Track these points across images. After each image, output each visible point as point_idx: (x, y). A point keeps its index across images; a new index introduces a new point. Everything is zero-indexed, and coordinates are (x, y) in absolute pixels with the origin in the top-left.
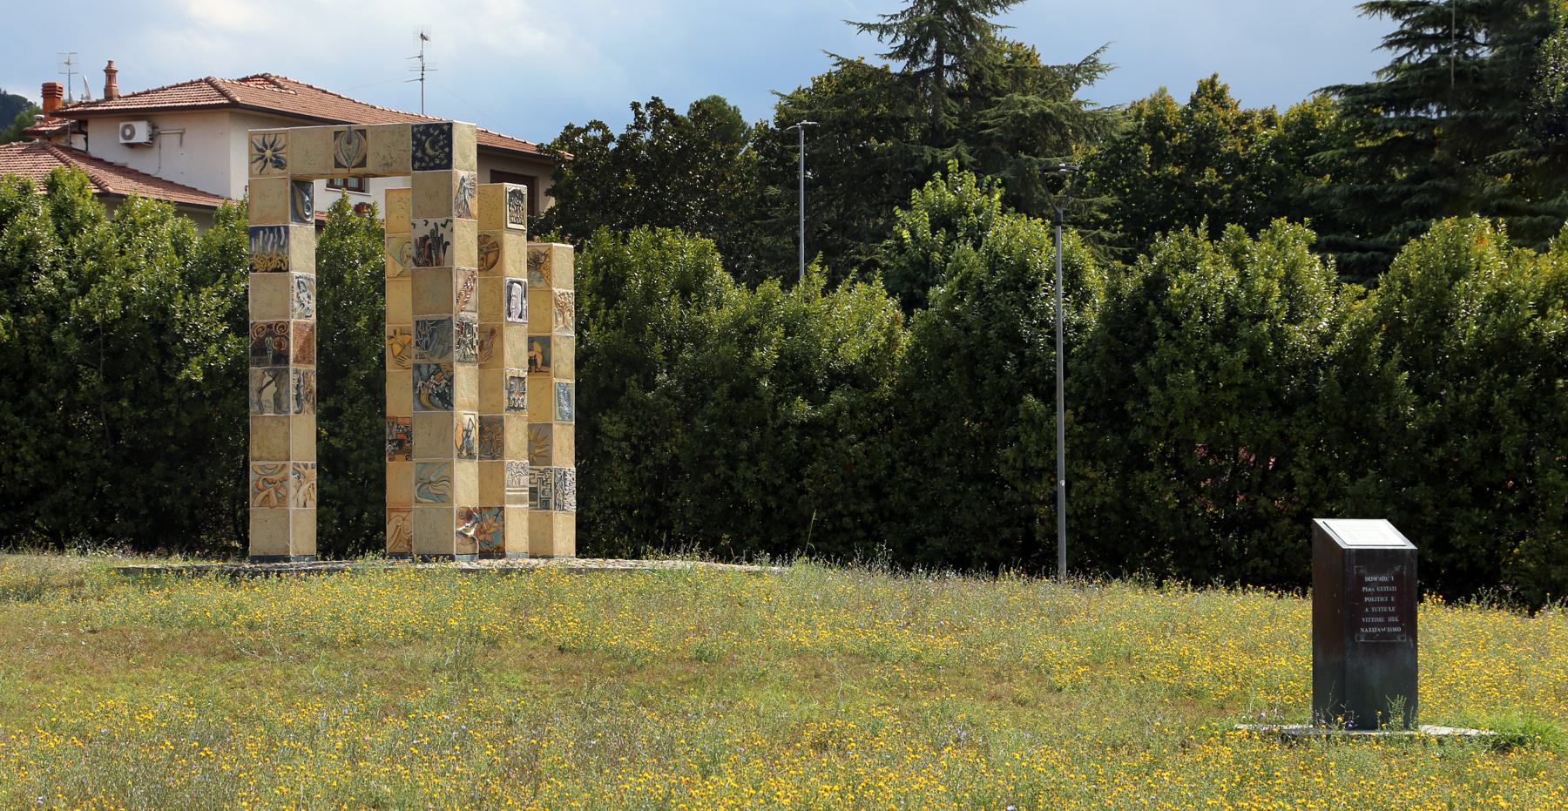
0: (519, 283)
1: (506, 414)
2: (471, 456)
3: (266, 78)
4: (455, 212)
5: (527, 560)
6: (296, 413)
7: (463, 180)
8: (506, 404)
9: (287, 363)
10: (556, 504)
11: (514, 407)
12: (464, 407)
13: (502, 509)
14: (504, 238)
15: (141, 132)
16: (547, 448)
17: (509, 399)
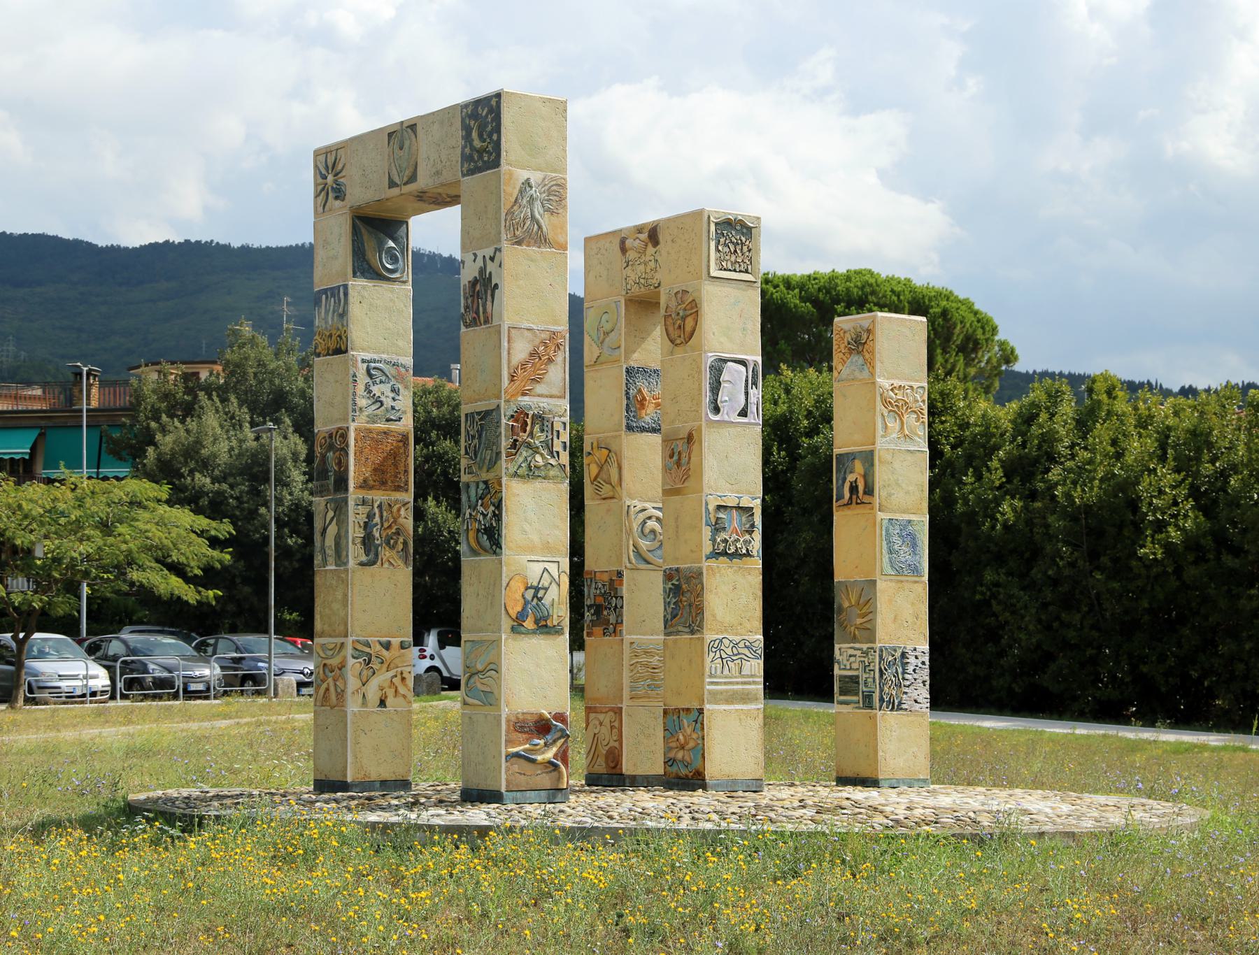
0: (743, 363)
1: (706, 564)
2: (544, 627)
6: (362, 564)
7: (527, 183)
8: (707, 548)
9: (346, 490)
10: (882, 700)
11: (724, 553)
12: (532, 550)
13: (701, 711)
14: (704, 293)
16: (870, 617)
17: (713, 540)
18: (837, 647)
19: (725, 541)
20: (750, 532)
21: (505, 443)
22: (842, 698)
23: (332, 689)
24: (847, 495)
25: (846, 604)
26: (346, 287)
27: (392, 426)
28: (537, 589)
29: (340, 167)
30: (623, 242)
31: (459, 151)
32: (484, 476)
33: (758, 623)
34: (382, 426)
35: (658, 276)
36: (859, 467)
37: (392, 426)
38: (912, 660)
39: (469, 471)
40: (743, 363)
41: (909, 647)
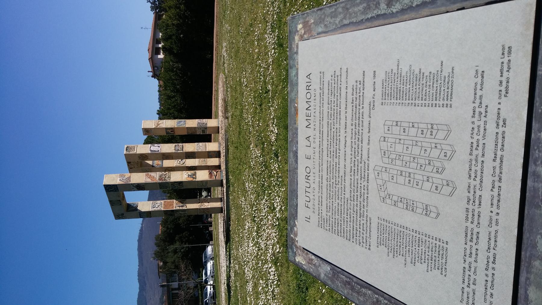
0: (150, 147)
2: (195, 174)
3: (148, 50)
4: (129, 183)
5: (220, 135)
11: (182, 149)
12: (182, 177)
13: (208, 152)
15: (156, 68)
17: (180, 150)
18: (198, 134)
19: (180, 149)
20: (179, 145)
21: (164, 181)
22: (206, 133)
23: (206, 211)
24: (173, 132)
25: (191, 132)
26: (139, 212)
27: (163, 204)
28: (189, 176)
29: (118, 215)
30: (130, 168)
31: (114, 192)
32: (170, 185)
33: (194, 144)
34: (163, 205)
35: (136, 162)
36: (168, 131)
37: (163, 204)
38: (199, 122)
39: (170, 188)
40: (150, 147)
41: (197, 122)
